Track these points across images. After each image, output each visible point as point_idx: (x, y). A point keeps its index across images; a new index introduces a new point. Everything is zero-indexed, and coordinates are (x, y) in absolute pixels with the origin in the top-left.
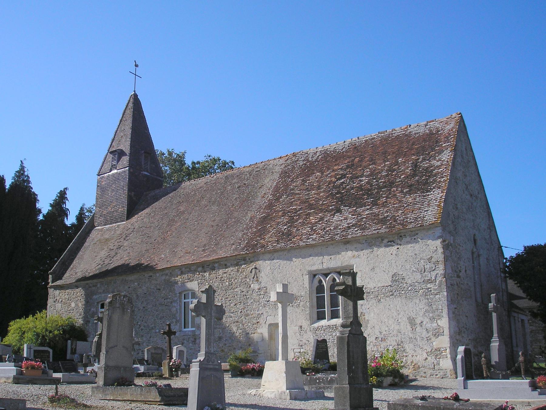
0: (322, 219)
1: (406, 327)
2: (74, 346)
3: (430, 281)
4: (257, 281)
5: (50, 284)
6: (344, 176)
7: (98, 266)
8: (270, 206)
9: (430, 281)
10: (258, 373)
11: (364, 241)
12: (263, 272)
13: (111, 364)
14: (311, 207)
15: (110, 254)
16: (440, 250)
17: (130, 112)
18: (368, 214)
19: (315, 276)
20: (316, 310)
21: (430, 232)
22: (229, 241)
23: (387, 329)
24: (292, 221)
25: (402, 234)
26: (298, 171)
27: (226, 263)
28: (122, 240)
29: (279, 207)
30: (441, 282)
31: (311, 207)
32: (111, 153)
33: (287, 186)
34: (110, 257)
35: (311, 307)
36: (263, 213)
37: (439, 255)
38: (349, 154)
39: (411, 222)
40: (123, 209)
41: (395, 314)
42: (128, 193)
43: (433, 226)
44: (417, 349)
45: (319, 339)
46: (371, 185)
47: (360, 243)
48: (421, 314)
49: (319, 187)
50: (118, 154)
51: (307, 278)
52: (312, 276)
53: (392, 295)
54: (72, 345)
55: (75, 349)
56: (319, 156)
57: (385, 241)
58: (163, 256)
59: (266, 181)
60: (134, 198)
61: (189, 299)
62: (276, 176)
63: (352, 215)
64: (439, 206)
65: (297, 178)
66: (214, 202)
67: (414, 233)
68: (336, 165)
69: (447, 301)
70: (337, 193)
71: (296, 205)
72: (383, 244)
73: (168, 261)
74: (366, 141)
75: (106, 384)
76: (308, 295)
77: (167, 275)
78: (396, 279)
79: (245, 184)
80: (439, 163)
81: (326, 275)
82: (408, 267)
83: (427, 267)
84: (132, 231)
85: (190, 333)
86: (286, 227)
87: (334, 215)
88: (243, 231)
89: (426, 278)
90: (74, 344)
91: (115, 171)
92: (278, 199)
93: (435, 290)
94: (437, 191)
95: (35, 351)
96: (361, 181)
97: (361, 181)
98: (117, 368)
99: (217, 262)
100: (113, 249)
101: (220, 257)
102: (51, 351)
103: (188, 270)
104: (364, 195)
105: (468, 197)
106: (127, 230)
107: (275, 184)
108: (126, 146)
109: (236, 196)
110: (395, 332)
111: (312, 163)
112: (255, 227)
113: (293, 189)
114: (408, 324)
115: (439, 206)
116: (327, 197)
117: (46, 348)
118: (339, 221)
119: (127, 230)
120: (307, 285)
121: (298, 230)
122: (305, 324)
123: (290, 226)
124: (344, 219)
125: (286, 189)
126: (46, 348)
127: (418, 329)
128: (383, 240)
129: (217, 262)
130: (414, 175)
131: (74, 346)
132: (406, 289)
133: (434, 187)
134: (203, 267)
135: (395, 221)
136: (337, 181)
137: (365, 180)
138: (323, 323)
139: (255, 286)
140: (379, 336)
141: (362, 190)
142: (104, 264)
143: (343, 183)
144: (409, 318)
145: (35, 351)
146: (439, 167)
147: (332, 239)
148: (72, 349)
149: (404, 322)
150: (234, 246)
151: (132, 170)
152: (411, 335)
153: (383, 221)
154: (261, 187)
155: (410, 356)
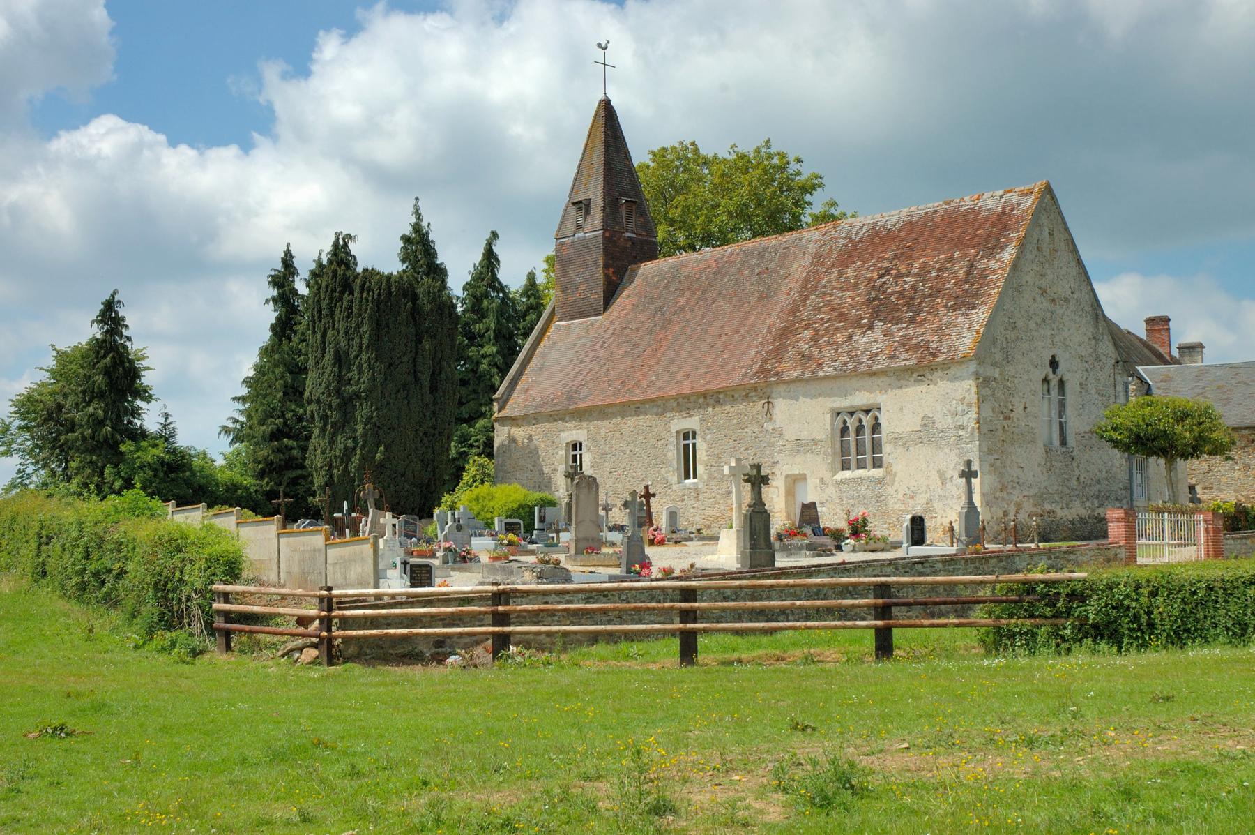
0: (850, 337)
1: (935, 482)
2: (542, 514)
3: (962, 427)
4: (771, 419)
5: (496, 415)
6: (888, 270)
7: (564, 388)
8: (794, 310)
9: (962, 427)
10: (715, 539)
11: (892, 374)
12: (777, 408)
13: (581, 536)
14: (842, 317)
15: (580, 370)
16: (974, 389)
17: (602, 113)
18: (901, 336)
19: (839, 414)
20: (839, 459)
21: (964, 366)
22: (739, 361)
23: (915, 484)
24: (815, 339)
25: (934, 367)
26: (835, 256)
27: (733, 393)
28: (598, 347)
29: (804, 314)
30: (973, 428)
31: (842, 317)
32: (574, 204)
33: (818, 280)
34: (581, 374)
35: (834, 454)
36: (785, 320)
37: (972, 396)
38: (902, 234)
39: (944, 353)
40: (598, 296)
41: (924, 465)
42: (604, 272)
43: (965, 359)
44: (948, 509)
45: (805, 503)
46: (916, 291)
47: (887, 375)
48: (952, 466)
49: (855, 286)
50: (582, 206)
51: (828, 417)
52: (835, 415)
53: (921, 442)
54: (540, 512)
55: (544, 517)
56: (865, 232)
57: (915, 375)
58: (654, 378)
59: (795, 267)
60: (614, 278)
61: (688, 439)
62: (807, 260)
63: (884, 335)
64: (978, 332)
65: (833, 267)
66: (725, 296)
67: (946, 366)
68: (882, 252)
69: (980, 451)
70: (875, 299)
71: (825, 313)
72: (912, 379)
73: (660, 387)
74: (926, 214)
75: (576, 553)
76: (829, 440)
77: (659, 406)
78: (928, 423)
79: (767, 269)
80: (996, 266)
81: (852, 414)
82: (939, 408)
83: (960, 409)
84: (612, 334)
85: (691, 487)
86: (807, 346)
87: (864, 333)
88: (757, 347)
89: (958, 424)
90: (543, 511)
91: (580, 235)
92: (804, 301)
93: (967, 438)
94: (985, 308)
95: (506, 524)
96: (905, 282)
97: (905, 282)
98: (586, 539)
99: (721, 392)
100: (585, 362)
101: (725, 385)
102: (521, 522)
103: (686, 400)
104: (904, 306)
105: (1046, 304)
106: (605, 331)
107: (805, 274)
108: (596, 194)
109: (753, 288)
110: (924, 488)
111: (855, 243)
112: (772, 343)
113: (825, 287)
114: (938, 479)
115: (978, 332)
116: (863, 303)
117: (517, 520)
118: (868, 343)
119: (605, 331)
120: (828, 427)
121: (820, 352)
122: (827, 475)
123: (812, 346)
124: (875, 341)
125: (816, 286)
126: (517, 520)
127: (949, 485)
128: (912, 373)
129: (721, 392)
130: (966, 281)
131: (542, 514)
132: (936, 435)
133: (981, 304)
134: (705, 398)
135: (928, 348)
136: (879, 278)
137: (911, 280)
138: (847, 474)
139: (769, 426)
140: (907, 492)
141: (904, 298)
142: (573, 385)
143: (885, 283)
144: (938, 471)
145: (506, 524)
146: (994, 271)
147: (855, 369)
148: (540, 517)
149: (934, 474)
150: (744, 370)
151: (607, 235)
152: (941, 493)
153: (914, 349)
154: (787, 277)
155: (939, 517)
